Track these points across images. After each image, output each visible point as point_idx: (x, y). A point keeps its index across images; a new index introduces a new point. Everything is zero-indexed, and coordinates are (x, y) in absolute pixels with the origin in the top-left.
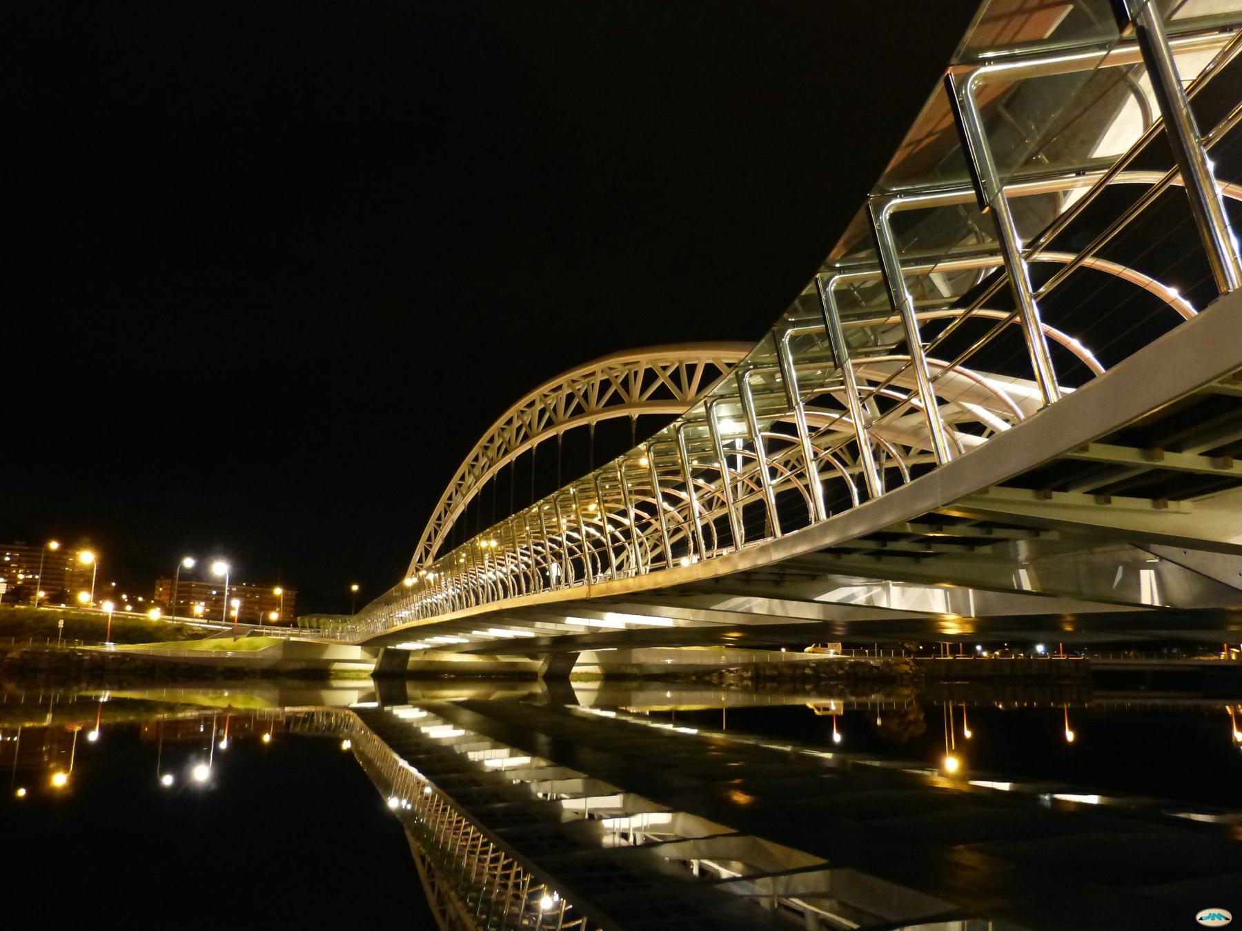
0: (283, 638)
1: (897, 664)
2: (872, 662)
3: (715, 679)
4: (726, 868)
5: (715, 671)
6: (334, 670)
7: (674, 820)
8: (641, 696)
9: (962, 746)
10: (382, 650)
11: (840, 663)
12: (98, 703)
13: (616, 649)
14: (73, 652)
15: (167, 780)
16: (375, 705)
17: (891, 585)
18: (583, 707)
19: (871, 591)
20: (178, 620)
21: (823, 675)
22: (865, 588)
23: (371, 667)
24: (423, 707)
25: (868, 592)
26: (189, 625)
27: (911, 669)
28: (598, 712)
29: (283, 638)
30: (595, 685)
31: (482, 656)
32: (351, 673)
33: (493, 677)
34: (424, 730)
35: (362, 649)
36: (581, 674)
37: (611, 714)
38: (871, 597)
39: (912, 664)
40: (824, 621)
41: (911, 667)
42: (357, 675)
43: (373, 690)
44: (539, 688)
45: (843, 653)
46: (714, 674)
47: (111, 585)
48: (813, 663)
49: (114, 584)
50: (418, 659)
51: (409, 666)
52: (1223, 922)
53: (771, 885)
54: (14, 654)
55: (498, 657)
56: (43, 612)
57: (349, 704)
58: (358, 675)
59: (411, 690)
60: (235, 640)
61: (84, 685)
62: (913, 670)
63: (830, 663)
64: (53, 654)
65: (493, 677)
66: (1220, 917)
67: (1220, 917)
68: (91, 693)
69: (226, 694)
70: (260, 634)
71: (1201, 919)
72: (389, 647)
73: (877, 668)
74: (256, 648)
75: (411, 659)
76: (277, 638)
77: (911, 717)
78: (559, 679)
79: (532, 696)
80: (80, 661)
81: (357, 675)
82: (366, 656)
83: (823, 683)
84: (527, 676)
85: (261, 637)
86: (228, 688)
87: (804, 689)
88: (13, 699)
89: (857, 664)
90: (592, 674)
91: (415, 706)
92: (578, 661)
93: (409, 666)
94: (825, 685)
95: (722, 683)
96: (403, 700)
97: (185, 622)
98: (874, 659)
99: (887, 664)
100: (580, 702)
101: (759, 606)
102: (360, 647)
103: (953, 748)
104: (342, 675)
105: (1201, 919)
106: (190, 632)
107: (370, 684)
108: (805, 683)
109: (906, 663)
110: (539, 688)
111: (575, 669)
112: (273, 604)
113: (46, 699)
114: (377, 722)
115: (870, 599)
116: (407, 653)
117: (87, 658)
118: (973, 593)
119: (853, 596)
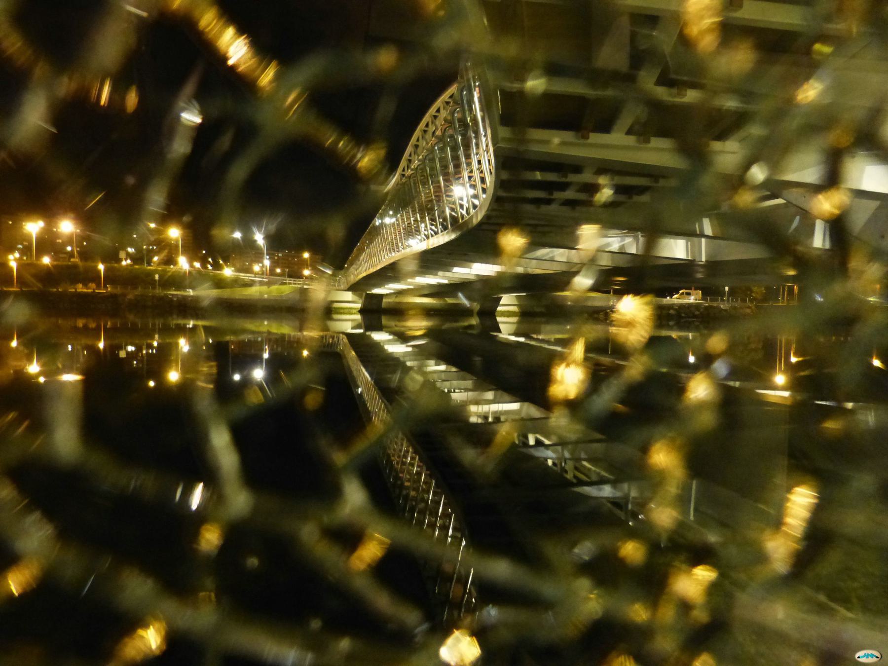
0: (299, 286)
1: (741, 308)
2: (722, 306)
3: (601, 316)
4: (547, 440)
5: (602, 311)
6: (334, 308)
7: (521, 407)
8: (548, 327)
9: (792, 369)
10: (364, 294)
11: (697, 306)
12: (186, 328)
13: (525, 294)
14: (166, 296)
15: (237, 377)
16: (361, 331)
17: (640, 236)
18: (503, 334)
19: (624, 241)
20: (242, 275)
21: (683, 315)
22: (619, 239)
23: (359, 306)
24: (391, 333)
25: (622, 241)
26: (242, 278)
27: (752, 312)
28: (513, 338)
29: (299, 286)
30: (514, 319)
31: (435, 299)
32: (345, 310)
33: (442, 313)
34: (386, 347)
35: (352, 293)
36: (505, 311)
37: (522, 339)
38: (623, 246)
39: (753, 308)
40: (614, 267)
41: (752, 310)
42: (349, 311)
43: (360, 321)
44: (474, 321)
45: (702, 300)
46: (601, 313)
47: (202, 253)
48: (677, 306)
49: (204, 252)
50: (390, 300)
51: (384, 305)
52: (875, 660)
53: (560, 451)
54: (130, 296)
55: (447, 299)
56: (150, 269)
57: (346, 330)
58: (350, 311)
59: (385, 321)
60: (268, 288)
61: (175, 316)
62: (754, 313)
63: (690, 305)
64: (154, 297)
65: (442, 313)
66: (872, 656)
67: (872, 656)
68: (181, 322)
69: (266, 323)
70: (284, 284)
71: (859, 657)
72: (368, 292)
73: (726, 310)
74: (282, 293)
75: (384, 300)
76: (296, 286)
77: (753, 346)
78: (489, 314)
79: (471, 327)
80: (171, 300)
81: (349, 311)
82: (356, 298)
83: (683, 320)
84: (466, 313)
85: (286, 286)
86: (268, 319)
87: (668, 325)
88: (134, 325)
89: (710, 307)
90: (512, 312)
91: (387, 332)
92: (501, 303)
93: (384, 305)
94: (685, 322)
95: (606, 319)
96: (379, 328)
97: (240, 276)
98: (724, 304)
99: (735, 308)
100: (502, 330)
101: (562, 255)
102: (350, 293)
103: (783, 369)
104: (340, 311)
105: (859, 657)
106: (242, 283)
107: (358, 317)
108: (669, 320)
109: (749, 307)
110: (474, 321)
111: (499, 309)
112: (303, 264)
113: (154, 325)
114: (357, 342)
115: (622, 247)
116: (381, 296)
117: (175, 299)
118: (705, 242)
119: (608, 245)
